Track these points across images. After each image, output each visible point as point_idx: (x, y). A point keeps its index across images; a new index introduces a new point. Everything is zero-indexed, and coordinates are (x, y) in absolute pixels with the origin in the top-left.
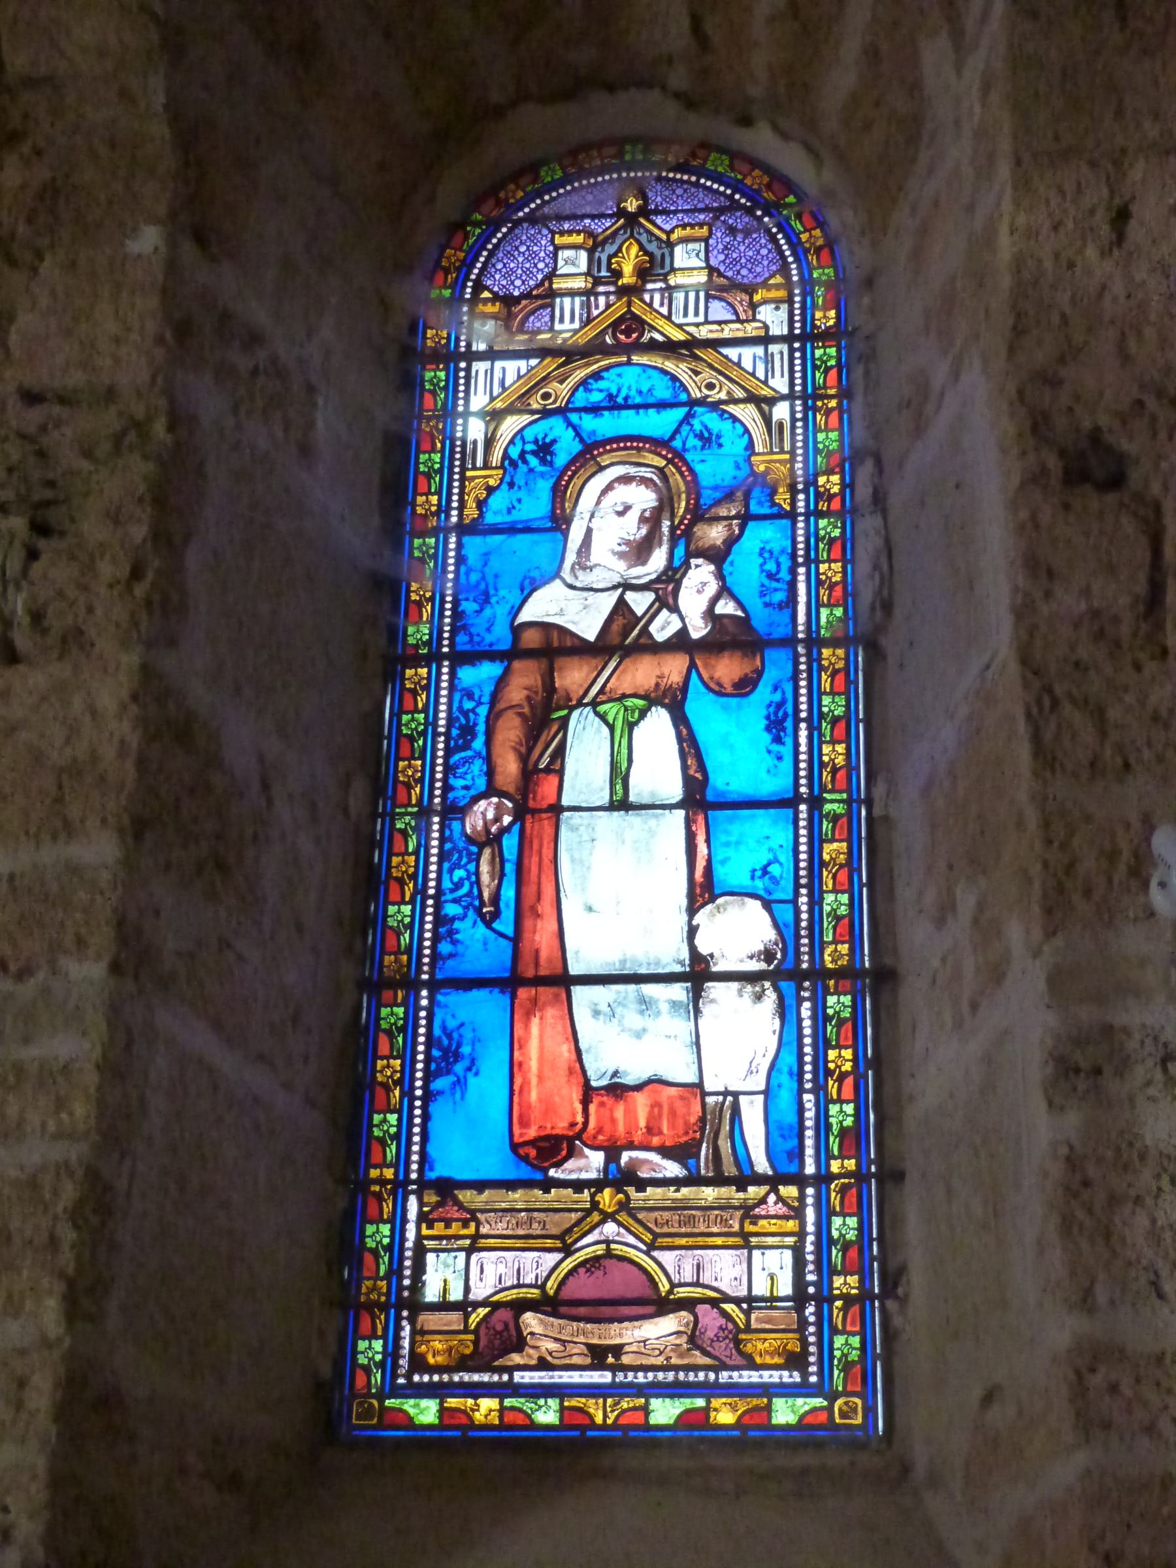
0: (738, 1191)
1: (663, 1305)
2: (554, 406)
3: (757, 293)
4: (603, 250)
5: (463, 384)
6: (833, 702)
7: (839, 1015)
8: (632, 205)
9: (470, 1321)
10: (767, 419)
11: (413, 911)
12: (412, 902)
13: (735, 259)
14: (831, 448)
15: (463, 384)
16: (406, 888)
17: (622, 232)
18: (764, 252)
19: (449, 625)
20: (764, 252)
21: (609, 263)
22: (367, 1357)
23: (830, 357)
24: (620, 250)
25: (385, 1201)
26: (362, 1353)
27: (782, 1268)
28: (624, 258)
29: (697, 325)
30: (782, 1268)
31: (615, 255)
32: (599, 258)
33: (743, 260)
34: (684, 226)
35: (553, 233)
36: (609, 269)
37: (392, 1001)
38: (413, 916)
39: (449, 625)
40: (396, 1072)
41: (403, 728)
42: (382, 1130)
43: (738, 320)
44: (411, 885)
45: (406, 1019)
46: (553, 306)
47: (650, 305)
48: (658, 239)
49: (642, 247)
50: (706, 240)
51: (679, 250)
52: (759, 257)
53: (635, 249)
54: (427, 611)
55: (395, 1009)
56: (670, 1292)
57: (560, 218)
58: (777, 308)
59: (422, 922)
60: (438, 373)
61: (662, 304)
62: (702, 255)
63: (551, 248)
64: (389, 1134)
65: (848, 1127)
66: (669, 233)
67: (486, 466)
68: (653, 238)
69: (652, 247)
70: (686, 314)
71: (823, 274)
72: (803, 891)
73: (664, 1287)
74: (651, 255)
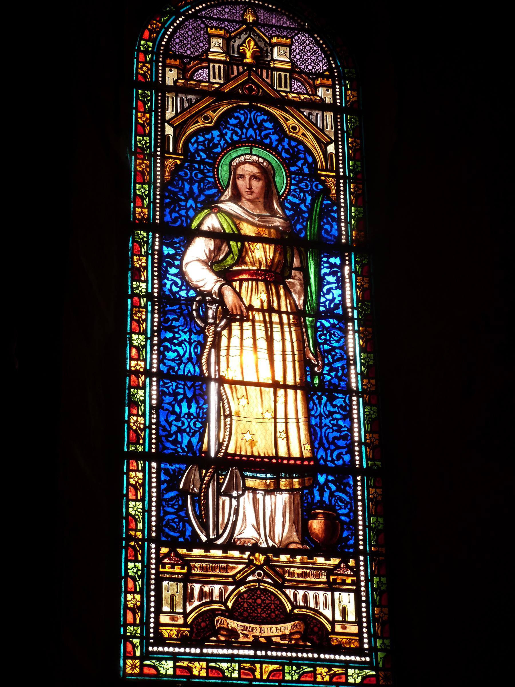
0: (326, 560)
1: (287, 617)
2: (210, 125)
3: (318, 80)
4: (235, 42)
5: (151, 602)
6: (363, 280)
7: (380, 588)
8: (250, 19)
9: (188, 619)
10: (325, 152)
11: (144, 476)
12: (148, 207)
13: (305, 59)
14: (379, 528)
15: (151, 602)
16: (145, 201)
17: (244, 33)
18: (320, 58)
19: (154, 574)
20: (320, 58)
21: (239, 49)
22: (135, 481)
23: (358, 166)
24: (244, 42)
25: (138, 581)
26: (132, 478)
27: (349, 602)
28: (247, 47)
29: (286, 92)
30: (349, 602)
31: (242, 45)
32: (233, 45)
33: (309, 61)
34: (278, 36)
35: (207, 26)
36: (239, 53)
37: (143, 133)
38: (144, 479)
39: (154, 574)
40: (139, 570)
41: (137, 191)
42: (138, 317)
43: (307, 94)
44: (147, 200)
45: (142, 601)
46: (208, 67)
47: (261, 76)
48: (264, 40)
49: (256, 44)
50: (290, 46)
51: (276, 50)
52: (318, 61)
53: (252, 44)
54: (140, 493)
55: (139, 363)
56: (292, 610)
57: (211, 18)
58: (328, 90)
59: (150, 482)
60: (143, 210)
61: (267, 78)
62: (288, 54)
63: (206, 36)
64: (139, 483)
65: (381, 529)
66: (270, 38)
67: (175, 152)
68: (261, 40)
69: (262, 45)
70: (280, 86)
71: (375, 465)
72: (342, 189)
73: (289, 607)
74: (261, 49)
